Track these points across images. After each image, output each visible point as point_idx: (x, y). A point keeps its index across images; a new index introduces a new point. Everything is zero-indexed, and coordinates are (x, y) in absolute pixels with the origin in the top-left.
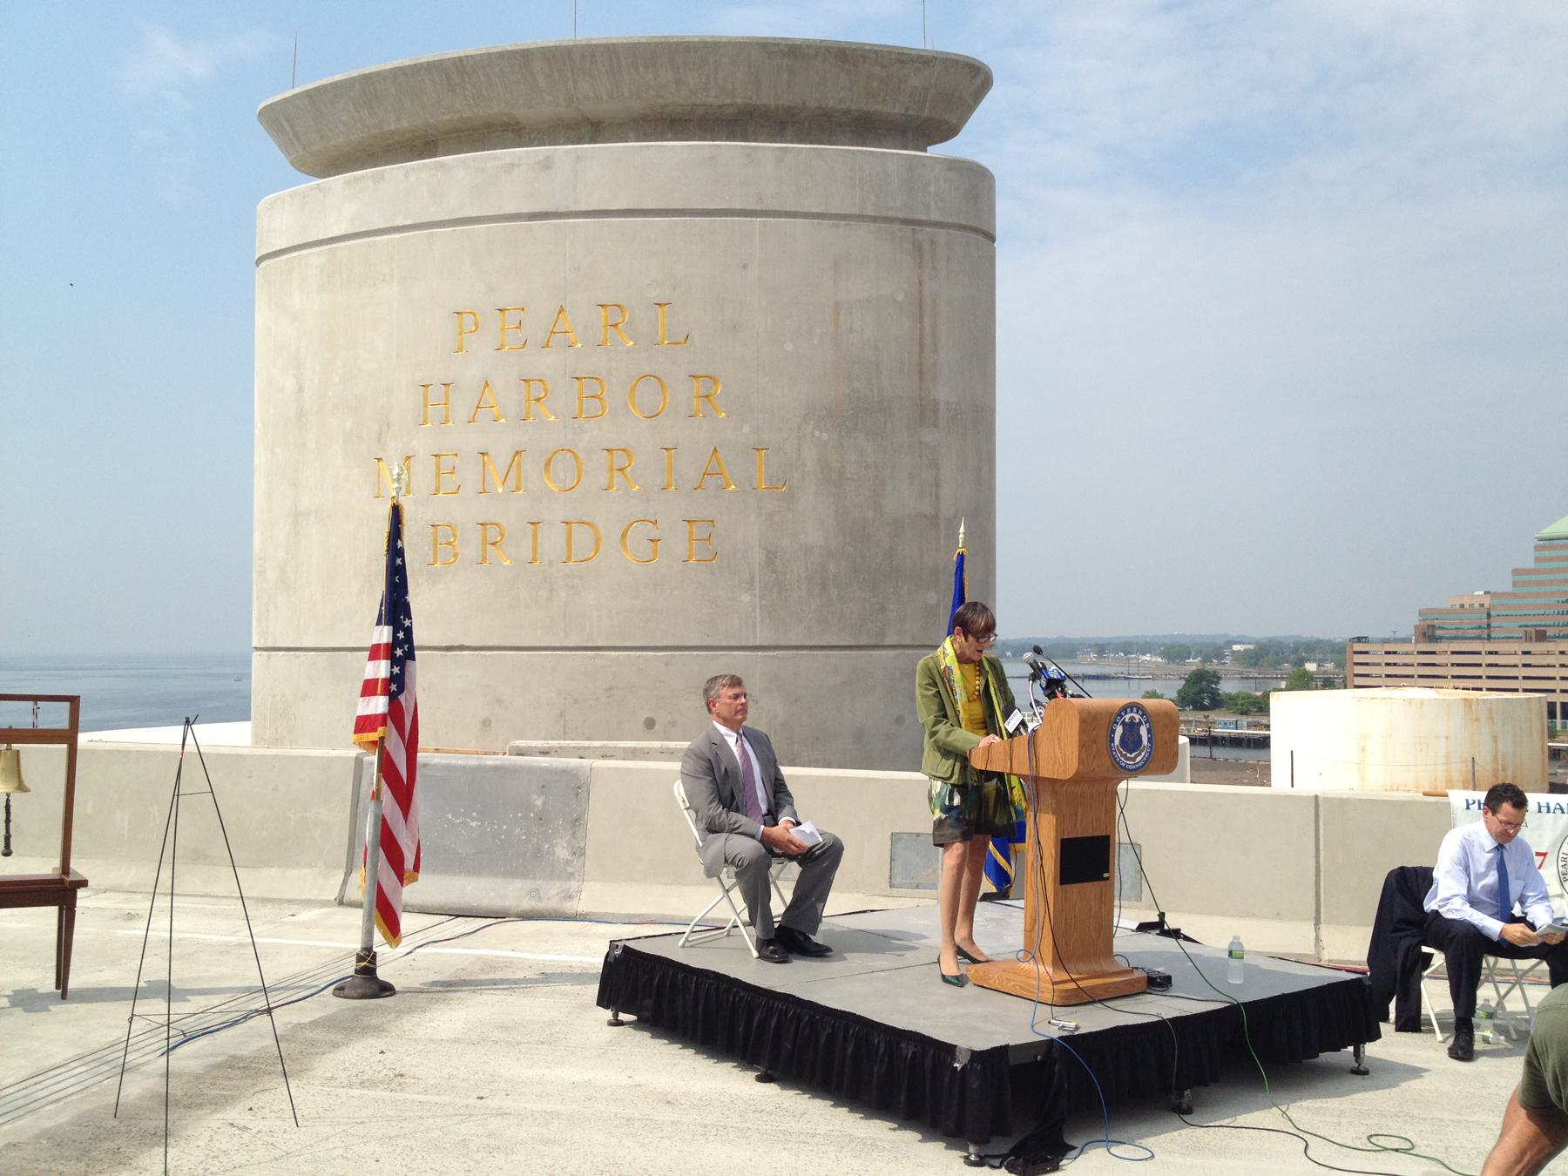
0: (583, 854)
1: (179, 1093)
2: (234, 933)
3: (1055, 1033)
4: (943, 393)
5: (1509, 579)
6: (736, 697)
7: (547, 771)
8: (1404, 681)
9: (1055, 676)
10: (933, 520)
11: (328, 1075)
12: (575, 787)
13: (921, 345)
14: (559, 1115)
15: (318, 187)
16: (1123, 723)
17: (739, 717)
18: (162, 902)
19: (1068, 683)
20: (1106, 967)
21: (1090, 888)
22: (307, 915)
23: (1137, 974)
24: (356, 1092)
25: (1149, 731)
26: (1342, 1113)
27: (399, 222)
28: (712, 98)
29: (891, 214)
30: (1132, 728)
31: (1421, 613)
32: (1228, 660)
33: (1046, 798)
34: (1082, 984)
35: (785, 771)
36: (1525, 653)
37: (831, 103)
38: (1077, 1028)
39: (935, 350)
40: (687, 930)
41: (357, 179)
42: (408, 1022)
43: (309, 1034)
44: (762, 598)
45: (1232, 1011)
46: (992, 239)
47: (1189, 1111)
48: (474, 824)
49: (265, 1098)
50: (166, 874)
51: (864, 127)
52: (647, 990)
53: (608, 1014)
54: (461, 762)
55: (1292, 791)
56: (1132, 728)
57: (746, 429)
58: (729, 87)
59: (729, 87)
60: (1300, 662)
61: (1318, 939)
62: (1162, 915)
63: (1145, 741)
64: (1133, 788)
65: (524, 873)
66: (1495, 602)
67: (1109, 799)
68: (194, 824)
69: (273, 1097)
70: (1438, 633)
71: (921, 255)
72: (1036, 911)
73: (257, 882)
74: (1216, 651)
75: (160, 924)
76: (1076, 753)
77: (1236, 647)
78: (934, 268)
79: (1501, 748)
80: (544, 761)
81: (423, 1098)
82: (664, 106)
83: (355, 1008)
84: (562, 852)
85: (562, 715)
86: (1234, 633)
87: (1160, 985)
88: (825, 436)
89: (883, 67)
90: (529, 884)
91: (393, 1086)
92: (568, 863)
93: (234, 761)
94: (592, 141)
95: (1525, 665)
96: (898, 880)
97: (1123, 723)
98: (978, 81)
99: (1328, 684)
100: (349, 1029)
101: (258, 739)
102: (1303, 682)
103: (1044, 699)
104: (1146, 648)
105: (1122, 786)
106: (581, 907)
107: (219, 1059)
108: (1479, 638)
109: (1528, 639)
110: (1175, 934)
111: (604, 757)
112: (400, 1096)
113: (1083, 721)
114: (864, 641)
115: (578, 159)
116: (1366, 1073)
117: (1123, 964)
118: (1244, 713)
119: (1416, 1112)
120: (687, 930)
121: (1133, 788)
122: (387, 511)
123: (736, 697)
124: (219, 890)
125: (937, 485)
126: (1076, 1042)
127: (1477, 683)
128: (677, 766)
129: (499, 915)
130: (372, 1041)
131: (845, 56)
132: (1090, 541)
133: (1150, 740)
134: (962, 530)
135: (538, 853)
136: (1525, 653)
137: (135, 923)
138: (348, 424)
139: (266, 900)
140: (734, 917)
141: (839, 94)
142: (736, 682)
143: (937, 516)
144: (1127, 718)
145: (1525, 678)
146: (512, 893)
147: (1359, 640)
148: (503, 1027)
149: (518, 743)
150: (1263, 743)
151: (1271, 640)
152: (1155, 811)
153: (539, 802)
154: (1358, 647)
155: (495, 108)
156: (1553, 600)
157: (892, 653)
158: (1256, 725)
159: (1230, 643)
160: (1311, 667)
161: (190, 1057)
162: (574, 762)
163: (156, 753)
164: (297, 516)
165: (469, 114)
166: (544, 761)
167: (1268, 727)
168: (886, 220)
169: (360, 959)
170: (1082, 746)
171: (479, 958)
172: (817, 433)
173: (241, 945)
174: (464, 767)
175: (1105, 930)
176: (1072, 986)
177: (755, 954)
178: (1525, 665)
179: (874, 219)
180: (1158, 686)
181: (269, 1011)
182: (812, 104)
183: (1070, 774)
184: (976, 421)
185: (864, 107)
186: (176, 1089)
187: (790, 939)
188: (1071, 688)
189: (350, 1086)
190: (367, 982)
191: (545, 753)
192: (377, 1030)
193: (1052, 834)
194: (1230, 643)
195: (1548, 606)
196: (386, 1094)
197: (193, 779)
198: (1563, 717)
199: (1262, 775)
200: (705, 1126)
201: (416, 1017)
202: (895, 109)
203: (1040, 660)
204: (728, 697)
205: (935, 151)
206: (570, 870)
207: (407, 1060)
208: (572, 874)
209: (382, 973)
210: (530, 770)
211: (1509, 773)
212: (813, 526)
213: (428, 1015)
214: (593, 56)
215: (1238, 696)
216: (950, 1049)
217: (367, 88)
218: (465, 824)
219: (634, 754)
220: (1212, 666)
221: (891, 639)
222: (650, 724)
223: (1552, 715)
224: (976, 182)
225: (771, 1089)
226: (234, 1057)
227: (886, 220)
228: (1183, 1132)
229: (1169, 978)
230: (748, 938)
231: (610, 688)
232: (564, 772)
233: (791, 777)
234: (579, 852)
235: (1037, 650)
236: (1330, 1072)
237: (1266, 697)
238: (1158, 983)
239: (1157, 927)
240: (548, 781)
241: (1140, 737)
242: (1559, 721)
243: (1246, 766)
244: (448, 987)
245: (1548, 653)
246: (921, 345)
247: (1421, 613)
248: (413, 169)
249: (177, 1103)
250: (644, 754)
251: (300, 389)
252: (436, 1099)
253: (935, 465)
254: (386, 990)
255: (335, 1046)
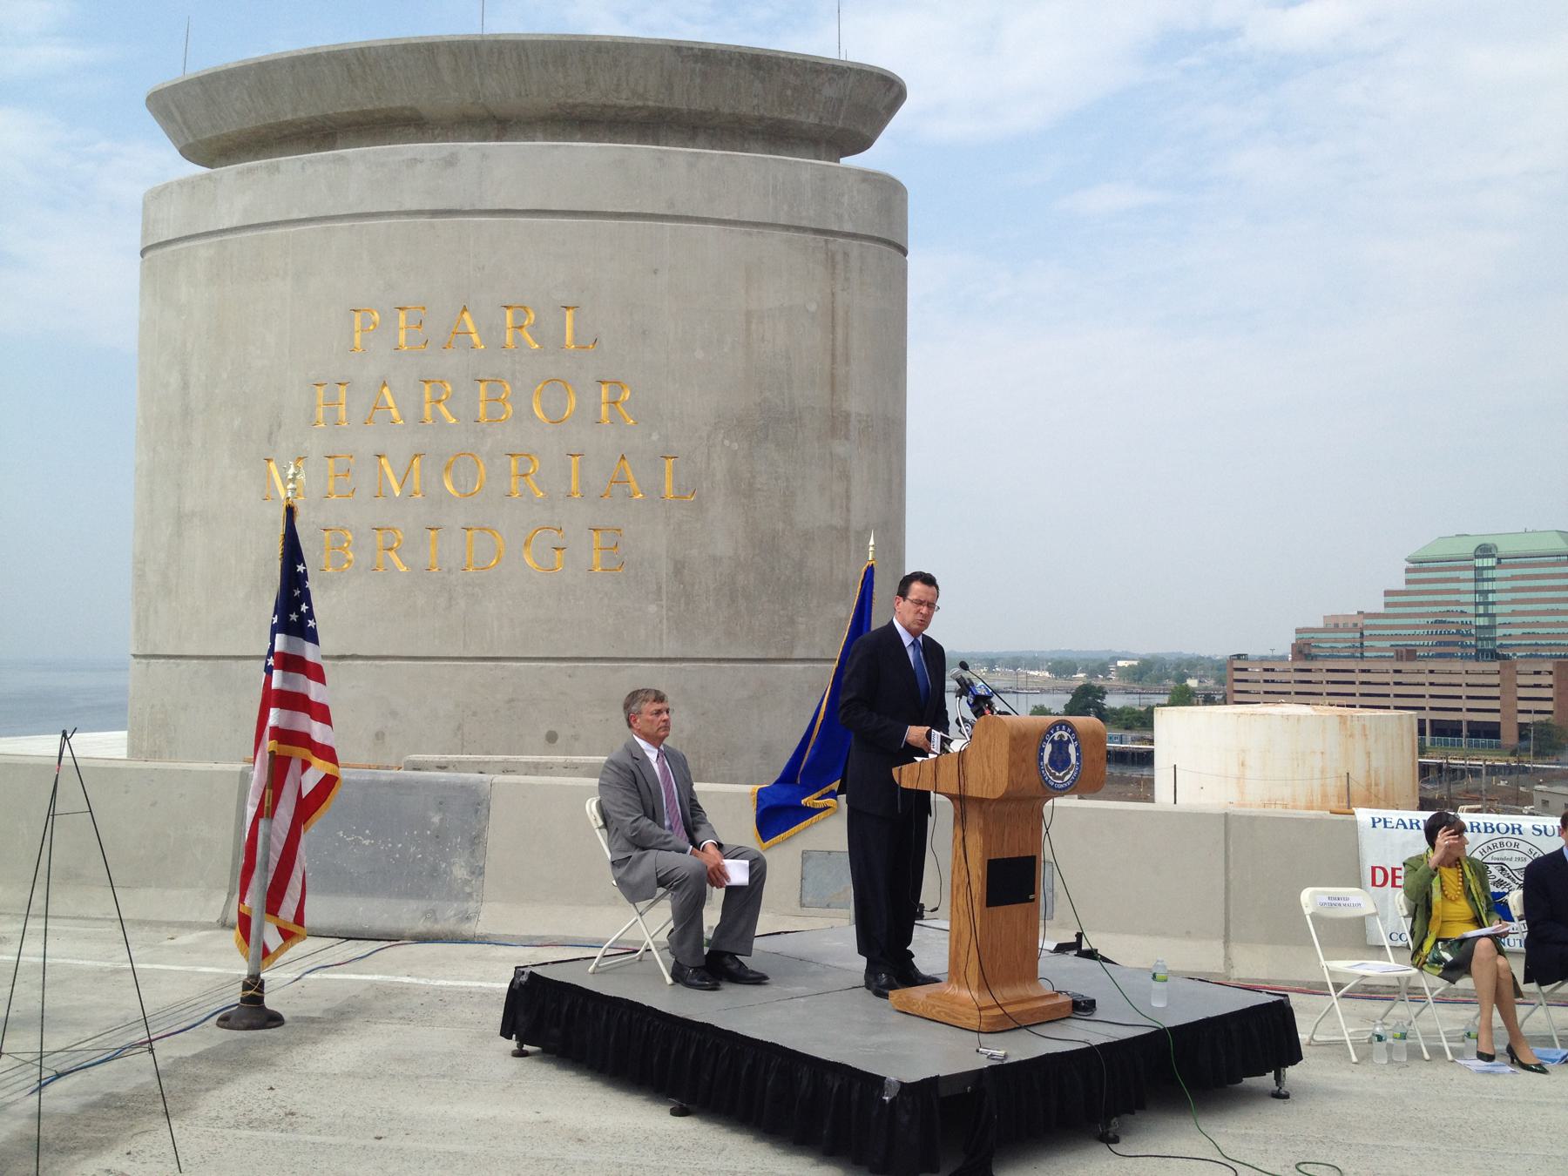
0: (482, 873)
1: (51, 1135)
2: (109, 958)
3: (984, 1063)
4: (855, 405)
5: (1382, 600)
6: (659, 712)
7: (445, 786)
8: (1282, 698)
9: (982, 692)
10: (844, 533)
11: (213, 1114)
12: (475, 803)
13: (833, 356)
14: (463, 1156)
15: (208, 177)
16: (1053, 741)
17: (662, 733)
18: (36, 925)
19: (995, 699)
20: (1031, 991)
21: (1016, 910)
22: (187, 938)
23: (1062, 999)
24: (246, 1133)
25: (1077, 749)
26: (1267, 1140)
27: (295, 216)
28: (623, 99)
29: (804, 223)
30: (1061, 746)
31: (1298, 631)
32: (1113, 676)
33: (974, 818)
34: (1009, 1010)
35: (697, 787)
36: (1396, 671)
37: (744, 109)
38: (1005, 1056)
39: (847, 362)
40: (599, 953)
41: (250, 170)
42: (298, 1055)
43: (191, 1070)
44: (669, 609)
45: (1159, 1036)
46: (904, 252)
47: (1116, 1140)
48: (367, 842)
49: (144, 1141)
50: (39, 893)
51: (777, 135)
52: (556, 1021)
53: (512, 1044)
54: (354, 778)
55: (1176, 808)
56: (1061, 746)
57: (655, 437)
58: (641, 90)
59: (641, 90)
60: (1182, 678)
61: (1227, 958)
62: (1079, 936)
63: (1073, 760)
64: (1064, 810)
65: (419, 893)
66: (1367, 622)
67: (1035, 819)
68: (71, 840)
69: (153, 1140)
70: (1314, 651)
71: (834, 267)
72: (959, 934)
73: (136, 903)
74: (1101, 667)
75: (33, 947)
76: (1006, 772)
77: (1120, 663)
78: (847, 279)
79: (1374, 764)
80: (442, 776)
81: (318, 1139)
82: (575, 106)
83: (240, 1041)
84: (460, 872)
85: (459, 727)
86: (1118, 649)
87: (1085, 1009)
88: (735, 446)
89: (796, 75)
90: (423, 905)
91: (283, 1126)
92: (467, 882)
93: (110, 773)
94: (498, 139)
95: (1396, 684)
96: (807, 899)
97: (1069, 741)
98: (896, 89)
99: (1209, 700)
100: (238, 1062)
101: (134, 751)
102: (1183, 697)
103: (970, 716)
104: (1034, 663)
105: (1049, 803)
106: (480, 928)
107: (95, 1098)
108: (1353, 657)
109: (1399, 657)
110: (1091, 954)
111: (505, 772)
112: (291, 1137)
113: (1013, 739)
114: (773, 654)
115: (484, 156)
116: (1287, 1096)
117: (1048, 990)
118: (1128, 728)
119: (1339, 1138)
120: (599, 953)
121: (1064, 810)
122: (282, 513)
123: (659, 712)
124: (94, 912)
125: (848, 497)
126: (1001, 1074)
127: (1351, 701)
128: (595, 782)
129: (394, 938)
130: (260, 1076)
131: (761, 64)
132: (1011, 558)
133: (1078, 759)
134: (872, 542)
135: (434, 873)
136: (1396, 671)
137: (6, 948)
138: (237, 423)
139: (142, 923)
140: (649, 940)
141: (753, 101)
142: (659, 698)
143: (847, 529)
144: (1056, 736)
145: (1432, 696)
146: (407, 914)
147: (1239, 656)
148: (400, 1060)
149: (414, 757)
150: (1146, 759)
151: (1154, 656)
152: (1073, 825)
153: (436, 819)
154: (1238, 664)
155: (398, 99)
156: (1423, 621)
157: (800, 666)
158: (1142, 740)
159: (1115, 659)
160: (1192, 683)
161: (61, 1097)
162: (473, 777)
163: (26, 766)
164: (181, 519)
165: (370, 107)
166: (442, 776)
167: (1151, 742)
168: (799, 229)
169: (246, 987)
170: (1012, 764)
171: (373, 984)
172: (727, 442)
173: (116, 971)
174: (355, 783)
175: (1032, 953)
176: (998, 1012)
177: (669, 980)
178: (1396, 684)
179: (787, 228)
180: (1046, 701)
181: (150, 1041)
182: (726, 110)
183: (999, 793)
184: (887, 433)
185: (776, 114)
186: (48, 1133)
187: (716, 963)
188: (999, 706)
189: (237, 1126)
190: (253, 1011)
191: (442, 768)
192: (266, 1063)
193: (979, 855)
194: (1115, 659)
195: (1418, 627)
196: (277, 1134)
197: (69, 786)
198: (1432, 734)
199: (1145, 791)
200: (620, 1166)
201: (308, 1049)
202: (808, 119)
203: (966, 675)
204: (643, 707)
205: (846, 161)
206: (468, 890)
207: (298, 1097)
208: (470, 894)
209: (271, 1002)
210: (427, 785)
211: (1382, 788)
212: (722, 535)
213: (320, 1047)
214: (500, 53)
215: (1122, 711)
216: (878, 1081)
217: (261, 75)
218: (357, 843)
219: (536, 769)
220: (1099, 681)
221: (798, 653)
222: (552, 737)
223: (1422, 732)
224: (889, 193)
225: (689, 1127)
226: (112, 1095)
227: (799, 229)
228: (1112, 1163)
229: (1094, 1002)
230: (663, 964)
231: (512, 700)
232: (464, 788)
233: (706, 793)
234: (478, 872)
235: (964, 666)
236: (1253, 1096)
237: (1150, 712)
238: (1083, 1007)
239: (1074, 947)
240: (444, 796)
241: (1068, 755)
242: (1428, 737)
243: (1129, 781)
244: (339, 1017)
245: (1419, 672)
246: (833, 356)
247: (1298, 631)
248: (310, 161)
249: (48, 1147)
250: (547, 769)
251: (185, 386)
252: (331, 1140)
253: (845, 476)
254: (275, 1020)
255: (220, 1082)
